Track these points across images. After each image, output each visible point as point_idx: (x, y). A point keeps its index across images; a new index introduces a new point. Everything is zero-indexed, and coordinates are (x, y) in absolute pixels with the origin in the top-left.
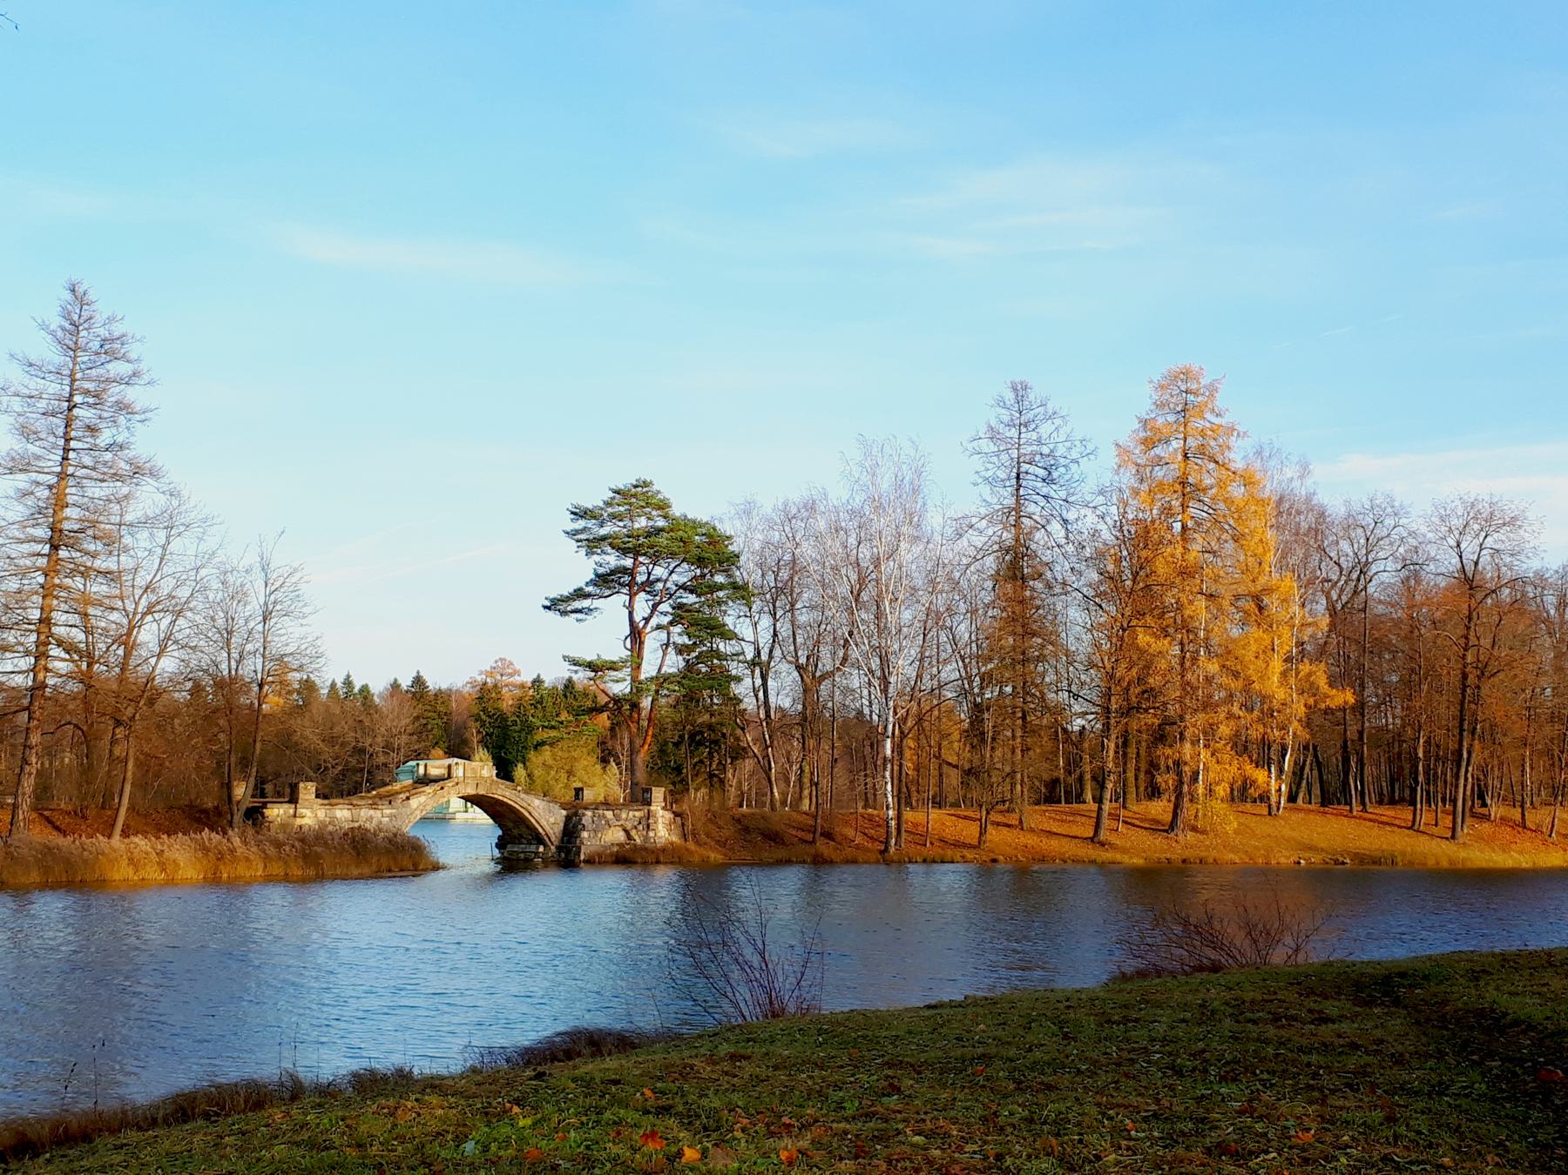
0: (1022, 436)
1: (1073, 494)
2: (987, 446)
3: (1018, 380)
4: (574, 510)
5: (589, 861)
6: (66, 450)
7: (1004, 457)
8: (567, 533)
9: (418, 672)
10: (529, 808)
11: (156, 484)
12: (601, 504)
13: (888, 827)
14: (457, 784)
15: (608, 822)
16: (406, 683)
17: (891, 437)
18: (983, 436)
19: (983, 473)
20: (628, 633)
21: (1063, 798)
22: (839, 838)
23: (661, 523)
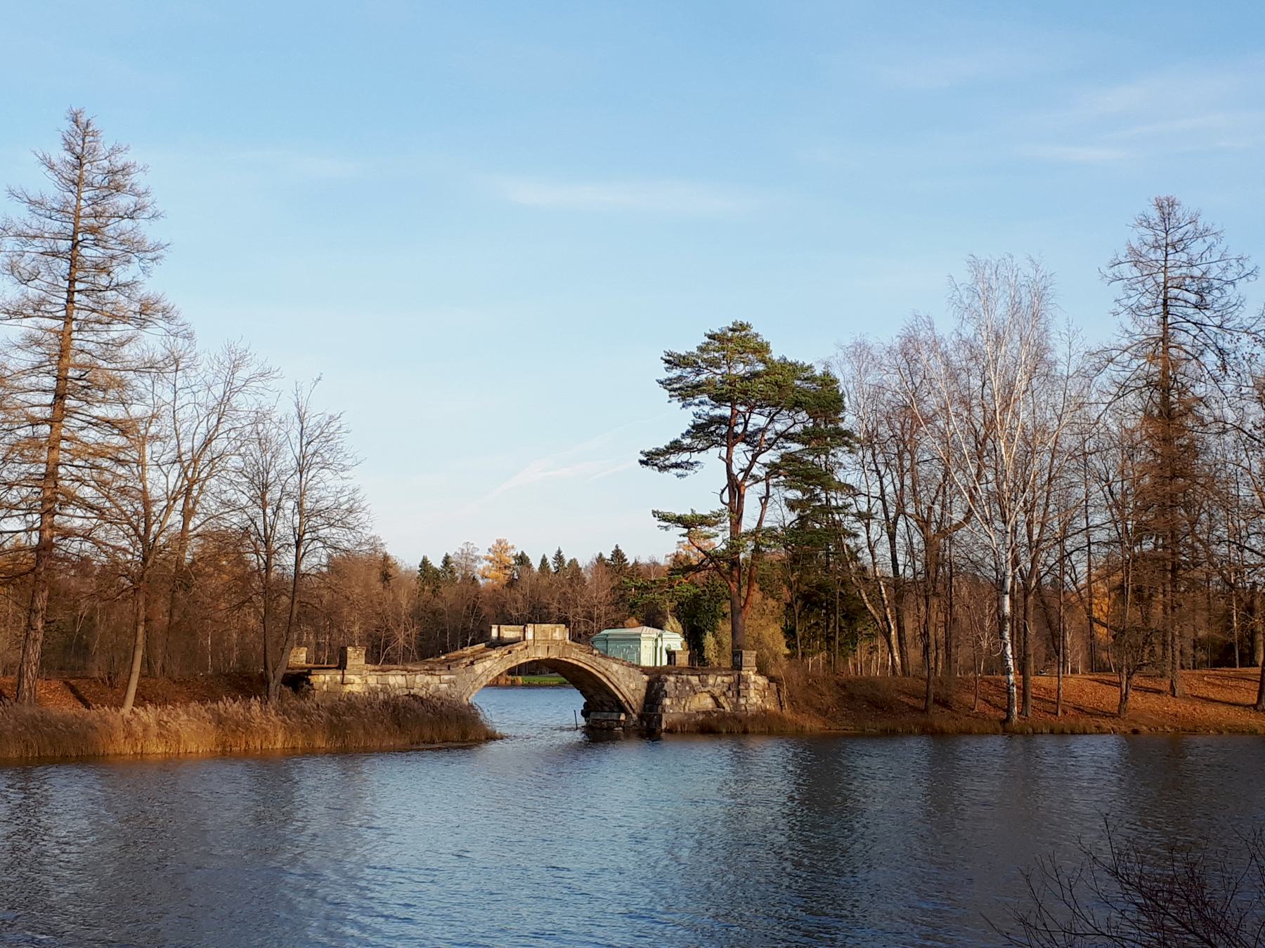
0: (1169, 257)
1: (1228, 320)
2: (1128, 271)
3: (1163, 196)
4: (668, 358)
5: (671, 731)
6: (70, 292)
7: (1150, 282)
8: (662, 383)
9: (617, 546)
10: (607, 673)
11: (167, 326)
12: (695, 351)
13: (1009, 694)
14: (526, 648)
15: (692, 687)
16: (608, 555)
17: (1006, 256)
18: (1123, 259)
19: (1125, 302)
20: (727, 482)
21: (1237, 662)
22: (956, 706)
23: (760, 367)
